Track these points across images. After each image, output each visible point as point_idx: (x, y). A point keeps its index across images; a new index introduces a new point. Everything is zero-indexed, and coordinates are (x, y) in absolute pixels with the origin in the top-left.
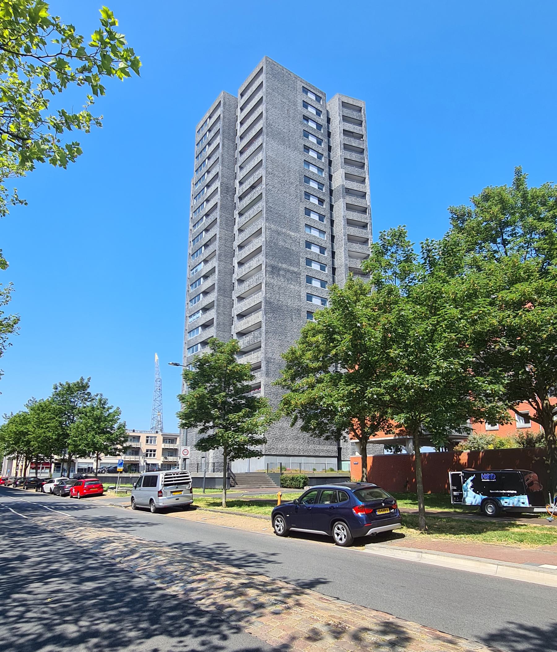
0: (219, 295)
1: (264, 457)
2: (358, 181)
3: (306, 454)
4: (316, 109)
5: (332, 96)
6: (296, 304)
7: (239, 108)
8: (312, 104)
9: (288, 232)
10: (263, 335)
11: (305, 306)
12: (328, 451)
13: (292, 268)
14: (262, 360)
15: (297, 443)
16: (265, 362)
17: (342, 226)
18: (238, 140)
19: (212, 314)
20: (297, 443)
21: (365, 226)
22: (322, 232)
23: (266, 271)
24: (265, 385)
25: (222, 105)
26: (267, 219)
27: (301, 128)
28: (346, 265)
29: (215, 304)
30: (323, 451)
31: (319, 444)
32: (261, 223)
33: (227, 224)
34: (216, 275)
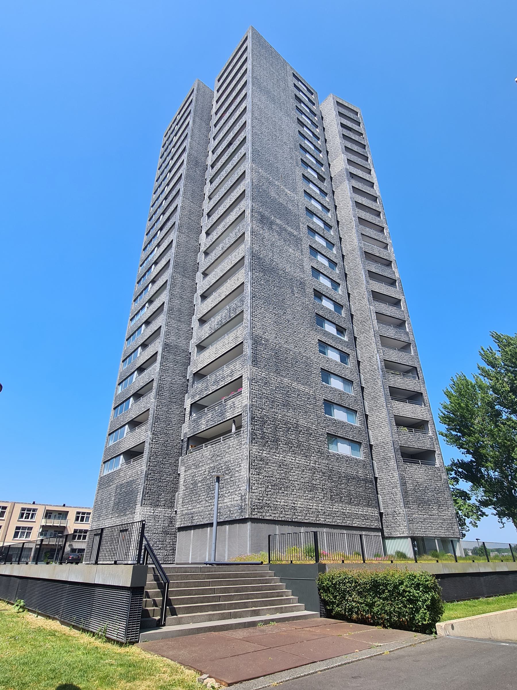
0: (174, 272)
1: (249, 524)
2: (387, 283)
3: (329, 521)
4: (341, 352)
5: (325, 97)
6: (298, 274)
7: (204, 232)
8: (325, 273)
9: (294, 384)
10: (248, 301)
11: (318, 360)
12: (365, 517)
13: (289, 229)
14: (245, 339)
15: (312, 498)
16: (250, 342)
17: (366, 300)
18: (197, 299)
19: (143, 434)
20: (312, 498)
21: (406, 347)
22: (348, 382)
23: (252, 216)
24: (251, 380)
25: (168, 287)
26: (253, 438)
27: (314, 338)
28: (361, 248)
29: (151, 417)
30: (357, 516)
31: (350, 503)
32: (241, 369)
33: (193, 196)
34: (157, 366)
